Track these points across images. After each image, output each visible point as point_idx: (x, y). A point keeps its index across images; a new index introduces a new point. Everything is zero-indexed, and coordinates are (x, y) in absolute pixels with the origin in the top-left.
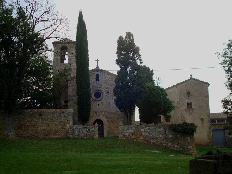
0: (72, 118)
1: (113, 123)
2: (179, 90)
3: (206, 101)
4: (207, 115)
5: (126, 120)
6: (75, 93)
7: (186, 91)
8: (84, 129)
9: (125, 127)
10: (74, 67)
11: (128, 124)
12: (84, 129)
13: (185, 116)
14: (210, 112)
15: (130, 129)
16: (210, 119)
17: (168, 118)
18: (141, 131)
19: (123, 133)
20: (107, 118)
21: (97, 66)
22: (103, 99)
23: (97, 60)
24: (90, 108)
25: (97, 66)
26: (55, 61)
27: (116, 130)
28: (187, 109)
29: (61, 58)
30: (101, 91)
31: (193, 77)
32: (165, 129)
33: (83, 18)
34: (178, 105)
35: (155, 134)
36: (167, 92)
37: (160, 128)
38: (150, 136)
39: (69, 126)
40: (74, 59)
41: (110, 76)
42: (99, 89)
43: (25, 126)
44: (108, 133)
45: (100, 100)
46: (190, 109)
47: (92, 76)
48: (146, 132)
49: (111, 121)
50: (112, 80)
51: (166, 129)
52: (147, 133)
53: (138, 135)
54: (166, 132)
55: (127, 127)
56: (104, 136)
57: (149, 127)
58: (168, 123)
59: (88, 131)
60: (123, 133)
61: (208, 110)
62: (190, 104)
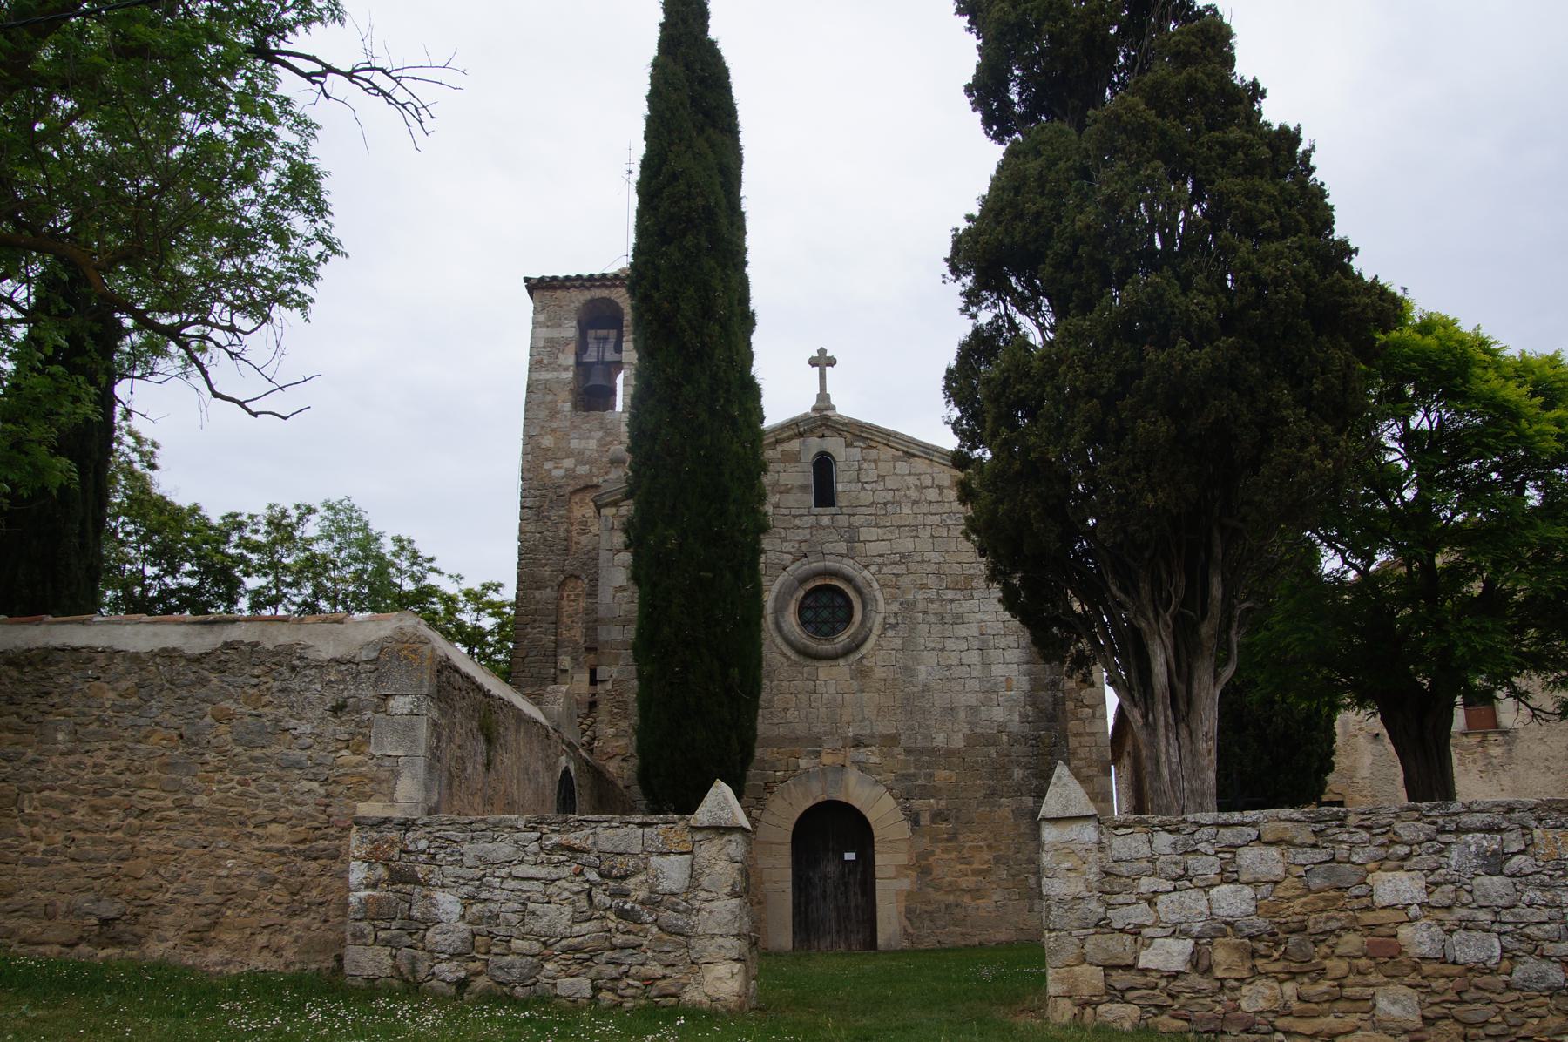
1: (953, 837)
8: (542, 872)
9: (1131, 845)
12: (542, 872)
15: (1206, 866)
18: (1384, 895)
20: (906, 793)
21: (823, 396)
23: (822, 361)
25: (823, 396)
26: (537, 397)
27: (975, 892)
30: (848, 580)
38: (1527, 968)
41: (920, 465)
42: (831, 563)
44: (910, 914)
45: (847, 652)
46: (1485, 734)
47: (779, 467)
48: (1450, 919)
50: (932, 494)
52: (1468, 925)
53: (1337, 967)
55: (1163, 840)
56: (880, 942)
57: (1489, 843)
59: (600, 897)
60: (1103, 925)
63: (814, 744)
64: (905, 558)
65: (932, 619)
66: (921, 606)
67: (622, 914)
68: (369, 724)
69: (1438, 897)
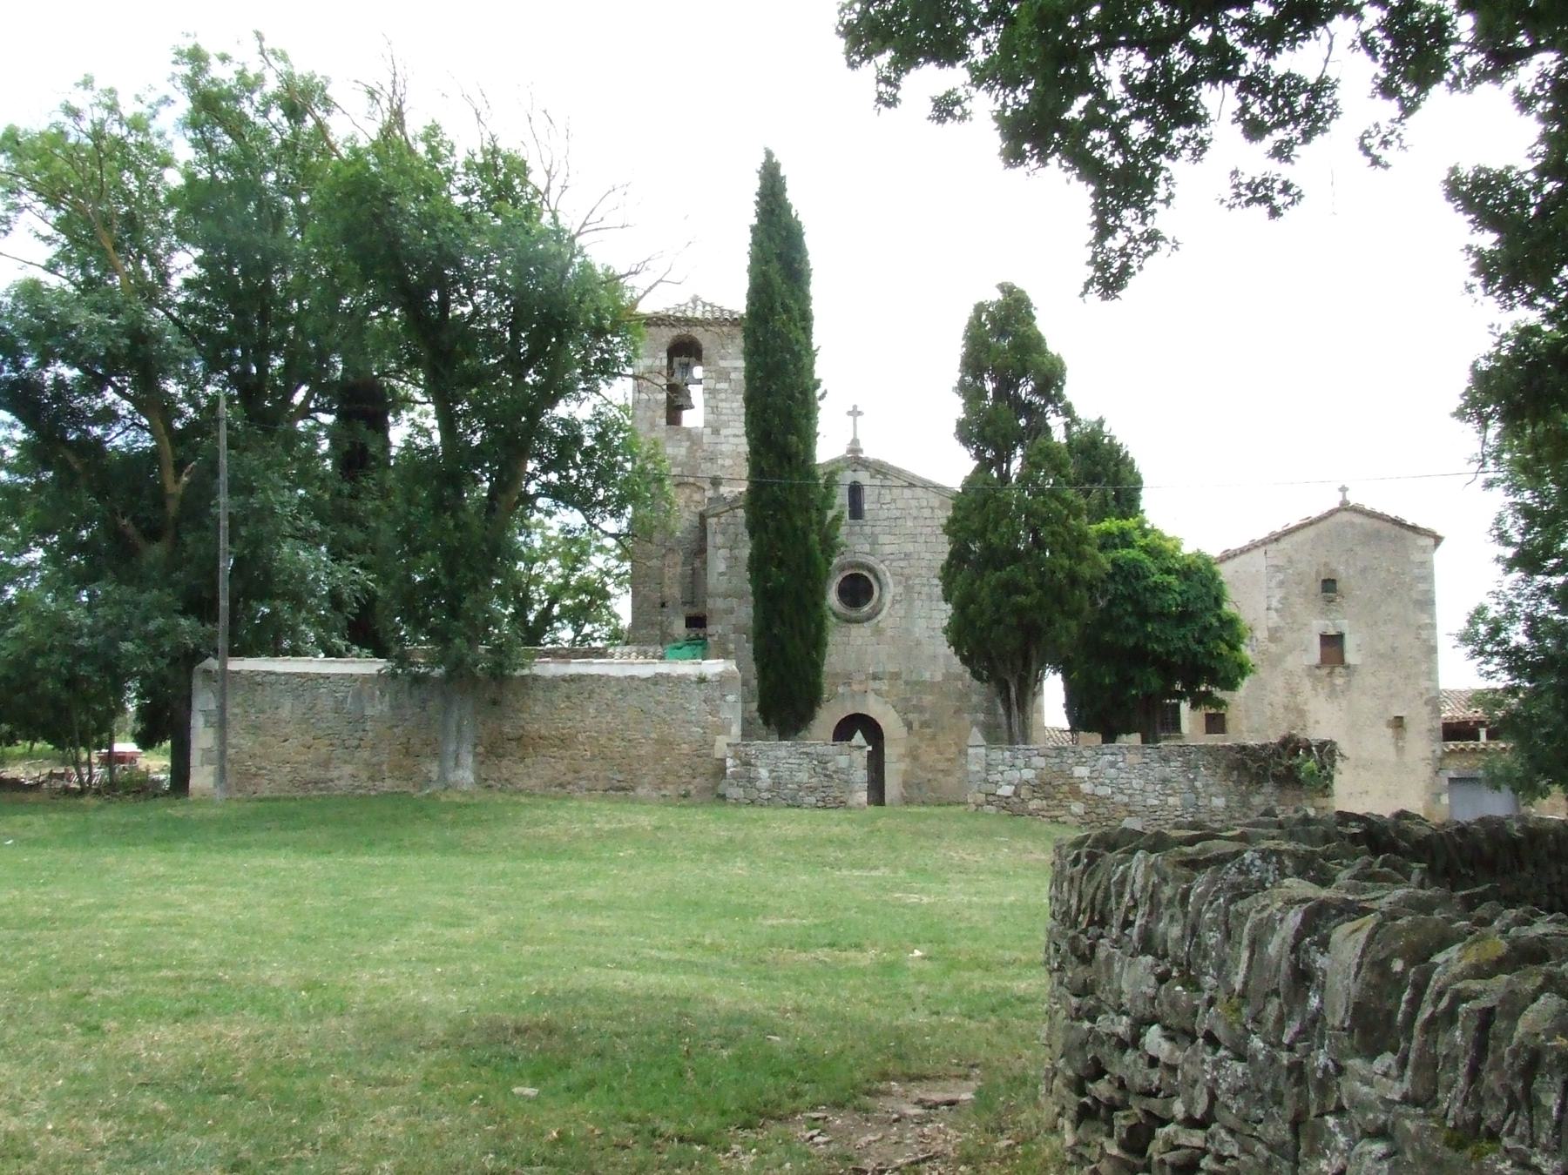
0: (739, 706)
1: (934, 737)
2: (1278, 568)
3: (1420, 627)
4: (1426, 703)
5: (1004, 720)
6: (743, 581)
7: (1318, 573)
9: (996, 755)
10: (737, 445)
11: (1012, 741)
13: (1306, 704)
14: (1441, 687)
15: (1020, 763)
16: (1439, 724)
17: (1216, 723)
18: (1076, 774)
19: (986, 781)
20: (904, 709)
22: (881, 610)
23: (855, 413)
24: (822, 656)
27: (946, 772)
28: (1318, 667)
29: (670, 401)
30: (871, 570)
31: (1353, 500)
32: (1189, 766)
33: (792, 195)
34: (1273, 648)
35: (1142, 790)
36: (1225, 572)
37: (1165, 760)
38: (1118, 798)
39: (728, 745)
40: (735, 408)
41: (919, 492)
43: (519, 739)
44: (906, 785)
45: (869, 618)
49: (925, 724)
50: (927, 513)
51: (1197, 767)
53: (1060, 796)
54: (1195, 779)
55: (1007, 754)
57: (1111, 758)
58: (1215, 740)
59: (818, 769)
60: (986, 781)
61: (1432, 674)
62: (1332, 644)
63: (847, 679)
64: (907, 556)
65: (924, 597)
66: (917, 588)
67: (826, 776)
68: (718, 706)
69: (1094, 775)
